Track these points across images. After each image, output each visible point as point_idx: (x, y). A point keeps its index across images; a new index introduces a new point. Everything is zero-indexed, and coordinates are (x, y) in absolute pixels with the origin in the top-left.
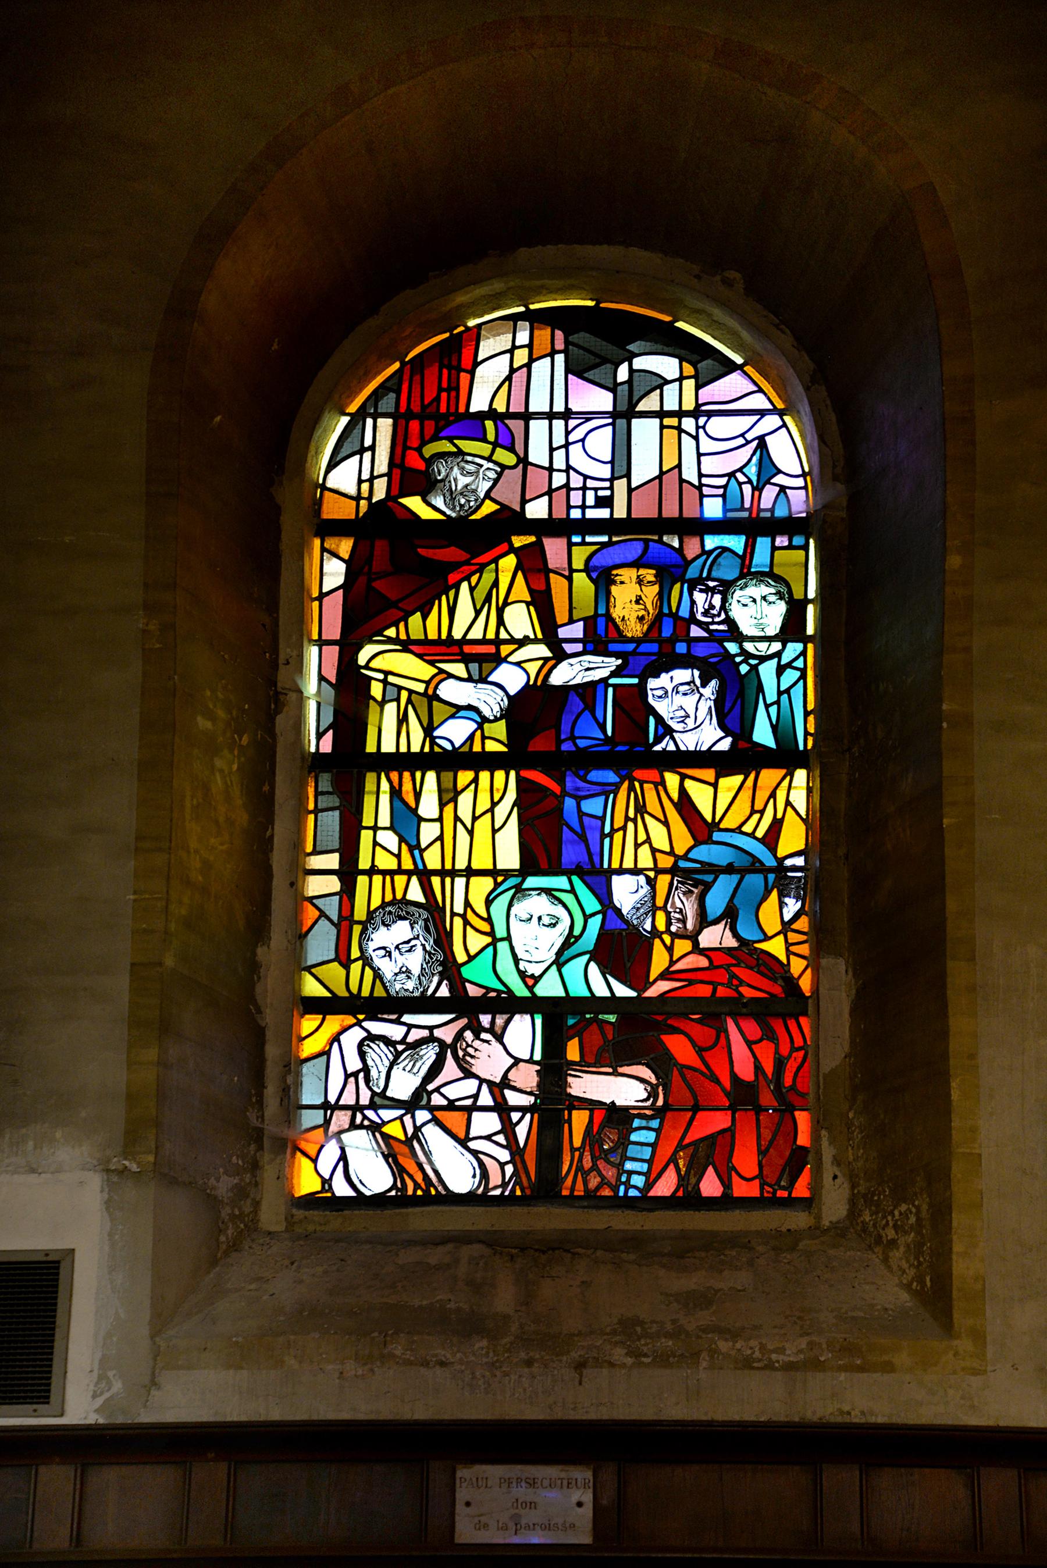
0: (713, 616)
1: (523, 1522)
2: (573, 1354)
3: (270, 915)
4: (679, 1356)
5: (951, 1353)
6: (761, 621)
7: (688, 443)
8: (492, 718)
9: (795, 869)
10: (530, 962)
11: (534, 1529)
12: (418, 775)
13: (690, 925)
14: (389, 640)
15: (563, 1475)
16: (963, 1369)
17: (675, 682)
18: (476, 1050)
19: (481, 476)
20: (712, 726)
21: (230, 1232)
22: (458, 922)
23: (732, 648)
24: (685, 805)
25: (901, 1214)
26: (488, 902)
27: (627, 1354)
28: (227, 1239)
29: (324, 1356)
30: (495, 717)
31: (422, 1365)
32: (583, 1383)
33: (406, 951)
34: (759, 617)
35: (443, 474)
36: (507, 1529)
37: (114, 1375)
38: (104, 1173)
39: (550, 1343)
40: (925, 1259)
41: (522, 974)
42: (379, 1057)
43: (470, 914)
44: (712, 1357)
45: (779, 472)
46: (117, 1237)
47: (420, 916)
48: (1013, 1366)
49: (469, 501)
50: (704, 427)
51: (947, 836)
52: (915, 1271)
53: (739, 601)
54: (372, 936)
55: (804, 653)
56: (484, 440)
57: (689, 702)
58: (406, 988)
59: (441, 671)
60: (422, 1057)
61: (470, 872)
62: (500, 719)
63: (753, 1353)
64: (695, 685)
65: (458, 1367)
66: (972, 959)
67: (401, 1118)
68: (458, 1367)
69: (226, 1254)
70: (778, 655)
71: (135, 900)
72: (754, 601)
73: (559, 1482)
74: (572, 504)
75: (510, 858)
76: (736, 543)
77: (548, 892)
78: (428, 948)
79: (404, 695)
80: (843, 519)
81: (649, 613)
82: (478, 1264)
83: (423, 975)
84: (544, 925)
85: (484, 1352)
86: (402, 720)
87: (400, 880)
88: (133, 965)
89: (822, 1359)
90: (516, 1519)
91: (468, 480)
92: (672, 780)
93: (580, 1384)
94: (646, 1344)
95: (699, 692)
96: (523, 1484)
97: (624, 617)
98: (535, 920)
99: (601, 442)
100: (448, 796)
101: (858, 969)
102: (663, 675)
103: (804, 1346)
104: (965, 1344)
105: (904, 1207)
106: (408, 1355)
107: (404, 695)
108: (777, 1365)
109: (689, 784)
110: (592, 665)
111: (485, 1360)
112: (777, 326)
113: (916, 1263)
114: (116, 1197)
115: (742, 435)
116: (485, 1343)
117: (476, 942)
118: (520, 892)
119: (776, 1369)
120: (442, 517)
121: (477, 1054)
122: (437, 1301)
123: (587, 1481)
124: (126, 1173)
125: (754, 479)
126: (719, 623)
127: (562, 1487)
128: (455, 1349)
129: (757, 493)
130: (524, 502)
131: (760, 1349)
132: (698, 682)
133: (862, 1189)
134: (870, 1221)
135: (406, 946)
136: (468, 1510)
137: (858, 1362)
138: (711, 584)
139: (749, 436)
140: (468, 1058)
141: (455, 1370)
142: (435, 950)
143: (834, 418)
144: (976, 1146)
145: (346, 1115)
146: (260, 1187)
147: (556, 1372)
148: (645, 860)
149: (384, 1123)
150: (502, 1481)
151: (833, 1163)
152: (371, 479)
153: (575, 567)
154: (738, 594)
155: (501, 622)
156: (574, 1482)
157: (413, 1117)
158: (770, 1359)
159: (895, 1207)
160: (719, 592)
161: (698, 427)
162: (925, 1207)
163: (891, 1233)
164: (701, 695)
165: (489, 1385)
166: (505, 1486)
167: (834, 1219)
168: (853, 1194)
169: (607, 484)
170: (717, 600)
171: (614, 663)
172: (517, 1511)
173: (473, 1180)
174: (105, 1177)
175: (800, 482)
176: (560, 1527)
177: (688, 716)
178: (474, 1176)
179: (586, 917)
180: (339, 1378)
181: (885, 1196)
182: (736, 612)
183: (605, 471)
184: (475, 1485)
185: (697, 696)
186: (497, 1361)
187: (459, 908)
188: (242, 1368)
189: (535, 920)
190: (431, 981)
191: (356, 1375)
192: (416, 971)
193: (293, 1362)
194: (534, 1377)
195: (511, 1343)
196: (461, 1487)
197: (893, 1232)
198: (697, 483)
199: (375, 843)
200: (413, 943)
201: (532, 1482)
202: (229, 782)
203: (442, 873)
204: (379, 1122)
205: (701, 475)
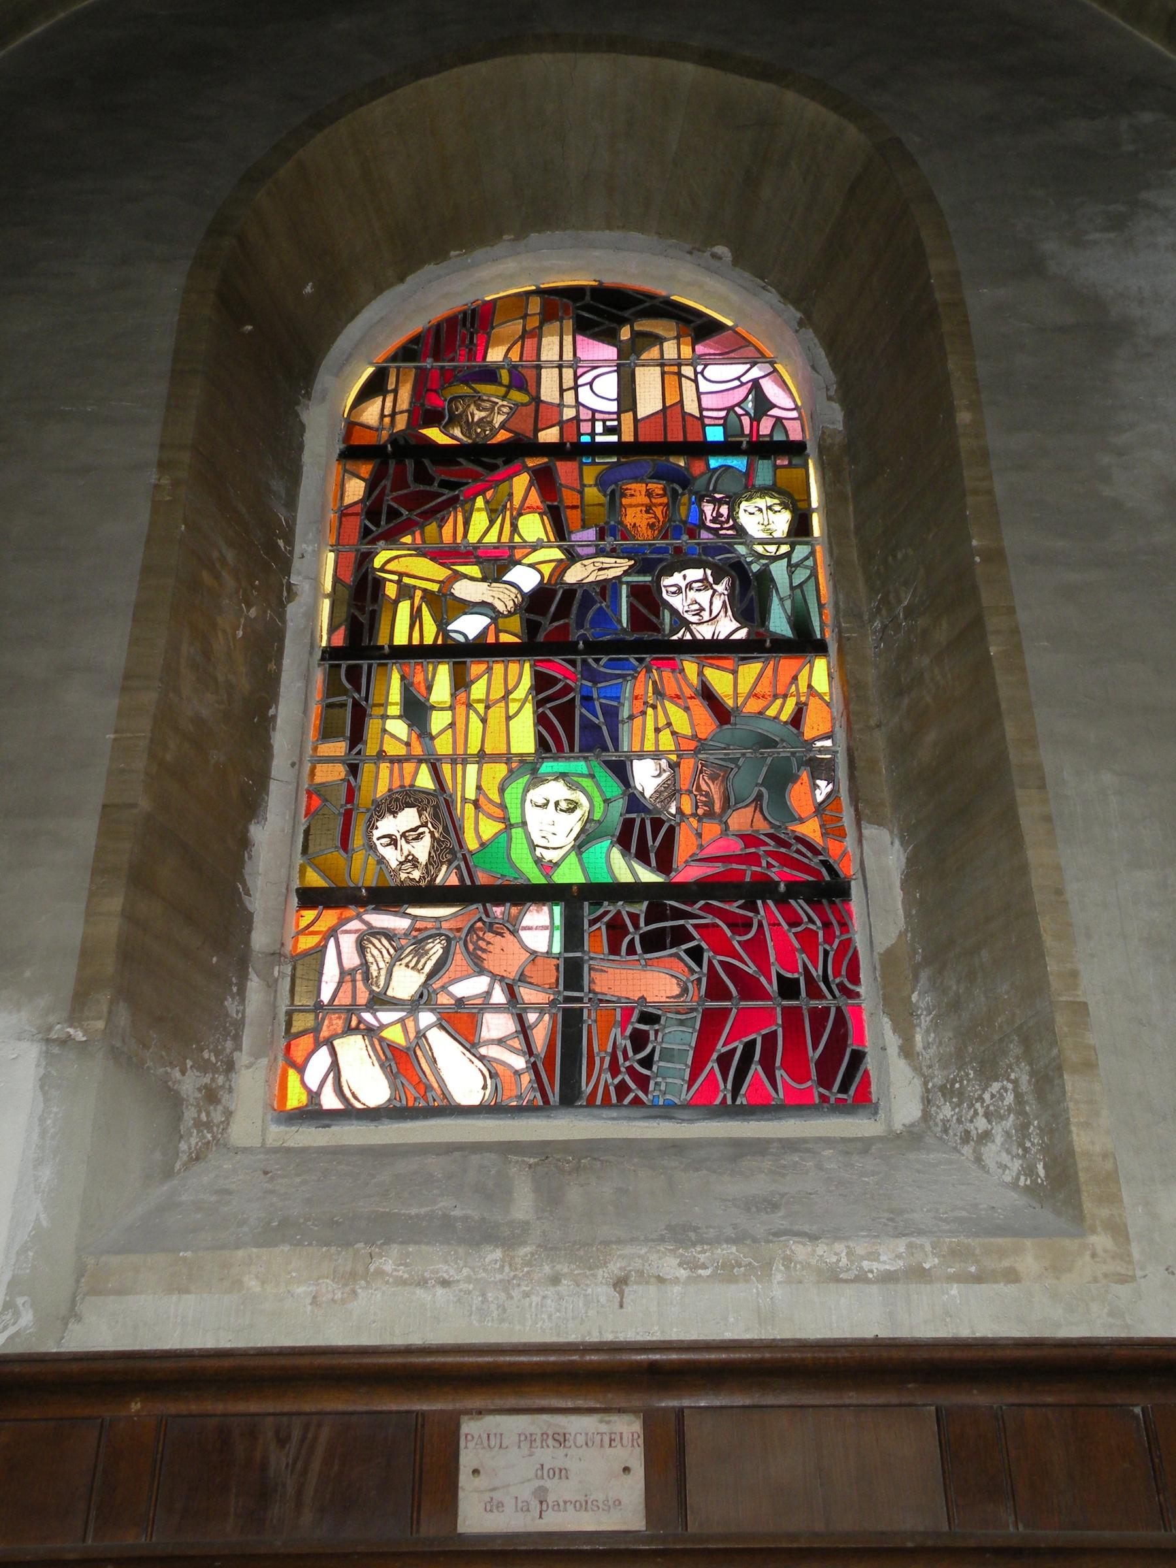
0: (722, 523)
1: (551, 1498)
2: (611, 1266)
3: (268, 795)
4: (746, 1266)
5: (1088, 1253)
6: (768, 527)
7: (688, 386)
8: (506, 613)
9: (823, 750)
10: (547, 848)
11: (565, 1510)
12: (431, 667)
13: (717, 807)
14: (405, 546)
15: (603, 1428)
16: (1106, 1276)
17: (688, 580)
18: (489, 943)
19: (496, 411)
20: (728, 619)
21: (193, 1141)
22: (470, 808)
23: (741, 549)
24: (707, 694)
25: (993, 1096)
26: (502, 790)
27: (680, 1265)
28: (190, 1148)
29: (294, 1275)
30: (509, 612)
31: (418, 1284)
32: (624, 1305)
33: (413, 839)
34: (766, 523)
35: (461, 409)
36: (528, 1510)
37: (24, 1304)
38: (44, 1043)
39: (582, 1253)
40: (1033, 1144)
41: (538, 861)
42: (379, 953)
43: (482, 801)
44: (787, 1268)
45: (774, 406)
46: (49, 1122)
47: (429, 802)
48: (1167, 1269)
49: (485, 431)
50: (702, 373)
51: (995, 664)
52: (1020, 1162)
53: (745, 511)
54: (378, 824)
55: (813, 553)
56: (501, 384)
57: (704, 597)
58: (411, 876)
59: (455, 571)
60: (427, 953)
61: (482, 757)
62: (514, 613)
63: (839, 1261)
64: (708, 582)
65: (464, 1286)
66: (1042, 787)
67: (401, 1021)
68: (464, 1286)
69: (186, 1166)
70: (788, 555)
71: (115, 740)
72: (760, 510)
73: (598, 1438)
74: (582, 431)
75: (524, 739)
76: (739, 463)
77: (562, 776)
78: (437, 835)
79: (419, 594)
80: (840, 432)
81: (659, 522)
82: (490, 1171)
83: (431, 864)
84: (561, 810)
85: (497, 1266)
86: (416, 616)
87: (409, 767)
88: (104, 806)
89: (927, 1266)
90: (541, 1496)
91: (483, 414)
92: (690, 668)
93: (621, 1306)
94: (703, 1252)
95: (712, 588)
96: (550, 1442)
97: (635, 524)
98: (551, 805)
99: (608, 385)
100: (461, 683)
101: (907, 835)
102: (676, 574)
103: (902, 1249)
104: (1101, 1241)
105: (995, 1087)
106: (402, 1272)
107: (419, 594)
108: (870, 1275)
109: (709, 673)
110: (605, 566)
111: (499, 1277)
112: (764, 288)
113: (1020, 1152)
114: (54, 1073)
115: (738, 378)
116: (498, 1254)
117: (489, 828)
118: (537, 780)
119: (867, 1281)
120: (455, 442)
121: (490, 948)
122: (440, 1209)
123: (636, 1436)
124: (69, 1043)
125: (752, 412)
126: (727, 529)
127: (602, 1446)
128: (461, 1263)
129: (755, 423)
130: (536, 431)
131: (847, 1254)
132: (711, 579)
133: (938, 1081)
134: (952, 1116)
135: (410, 836)
136: (477, 1482)
137: (973, 1269)
138: (718, 496)
139: (744, 379)
140: (479, 953)
141: (461, 1290)
142: (444, 837)
143: (823, 354)
144: (1080, 993)
145: (339, 1018)
146: (235, 1095)
147: (589, 1291)
148: (666, 742)
149: (383, 1027)
150: (523, 1438)
151: (899, 1055)
152: (393, 415)
153: (586, 482)
154: (744, 505)
155: (514, 528)
156: (618, 1439)
157: (416, 1021)
158: (861, 1268)
159: (984, 1090)
160: (727, 503)
161: (696, 373)
162: (1025, 1079)
163: (981, 1124)
164: (715, 591)
165: (504, 1310)
166: (525, 1446)
167: (907, 1121)
168: (928, 1091)
169: (615, 416)
170: (724, 510)
171: (626, 563)
172: (541, 1483)
173: (483, 1092)
174: (44, 1048)
175: (794, 414)
176: (601, 1505)
177: (702, 609)
178: (485, 1087)
179: (607, 801)
180: (311, 1304)
181: (969, 1081)
182: (744, 519)
183: (613, 407)
184: (486, 1443)
185: (711, 592)
186: (515, 1277)
187: (471, 794)
188: (188, 1292)
189: (551, 805)
190: (440, 870)
191: (333, 1300)
192: (423, 858)
193: (253, 1283)
194: (561, 1298)
195: (532, 1254)
196: (466, 1447)
197: (984, 1120)
198: (698, 415)
199: (384, 731)
200: (421, 830)
201: (562, 1440)
202: (232, 647)
203: (453, 760)
204: (376, 1024)
205: (701, 409)
